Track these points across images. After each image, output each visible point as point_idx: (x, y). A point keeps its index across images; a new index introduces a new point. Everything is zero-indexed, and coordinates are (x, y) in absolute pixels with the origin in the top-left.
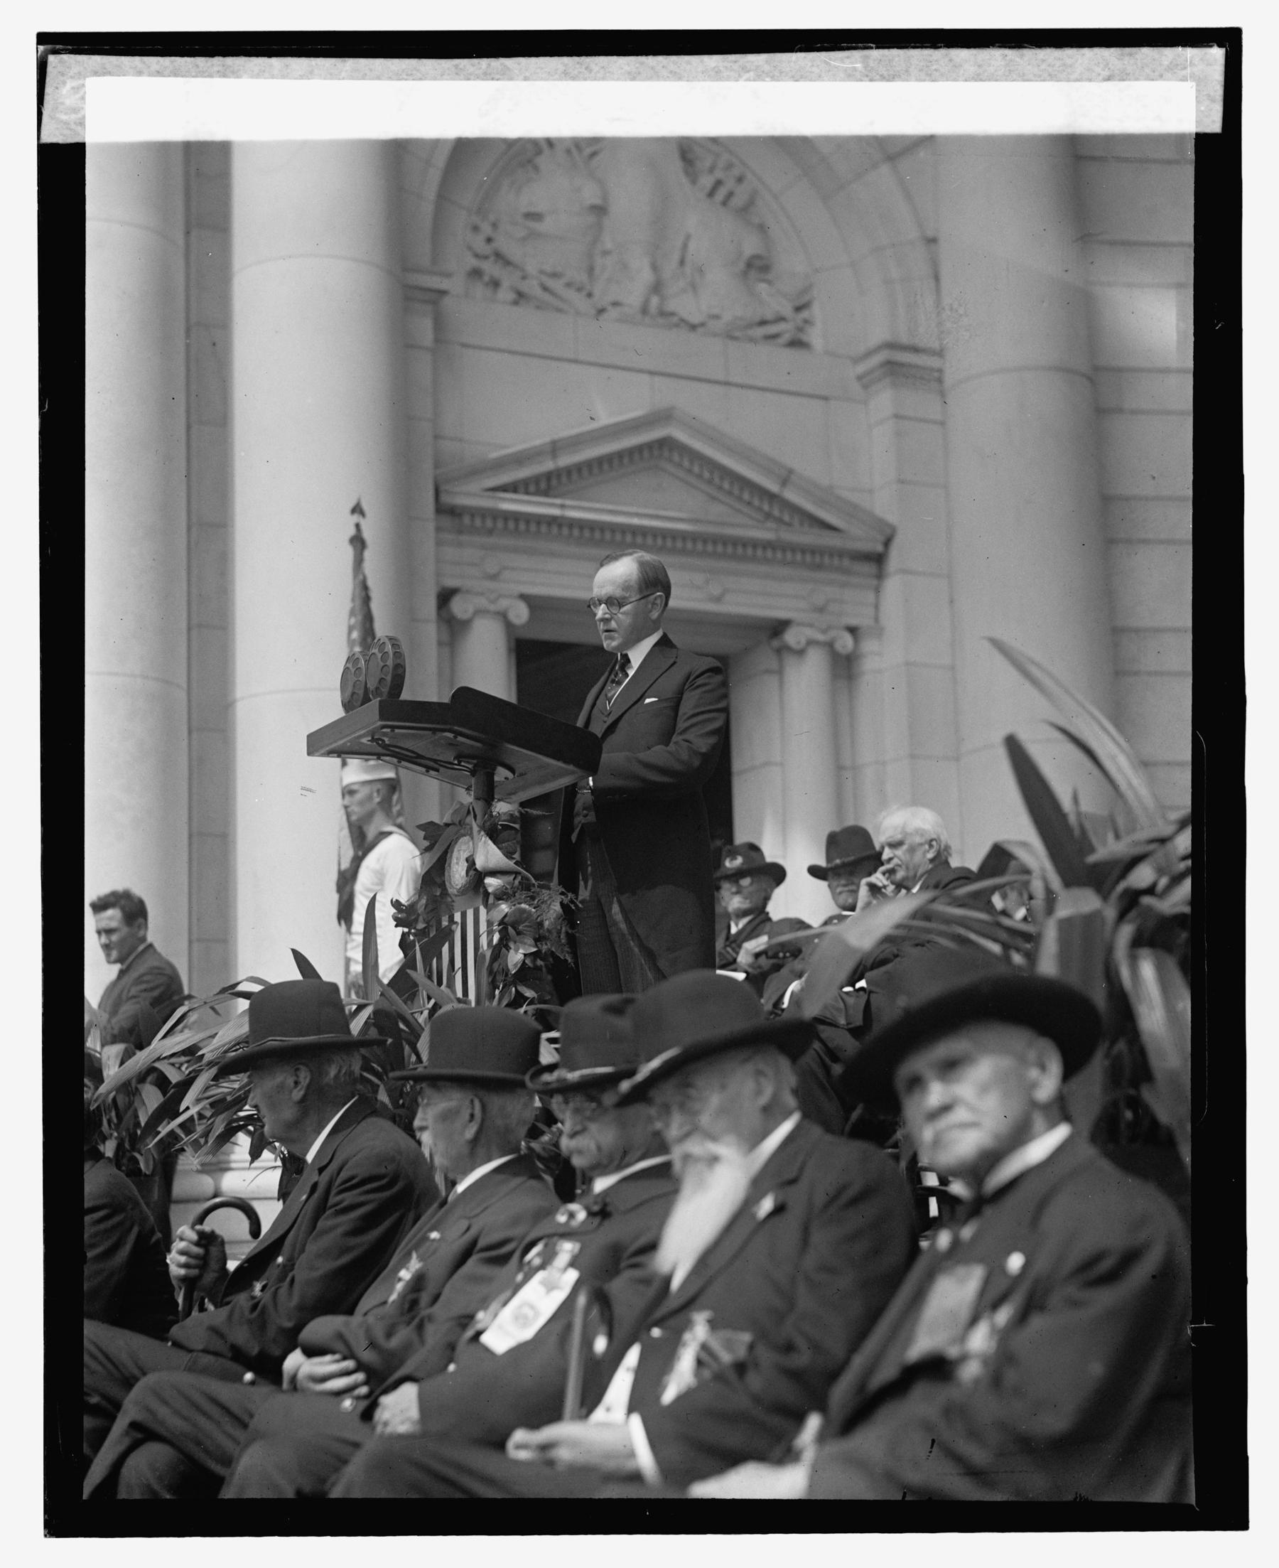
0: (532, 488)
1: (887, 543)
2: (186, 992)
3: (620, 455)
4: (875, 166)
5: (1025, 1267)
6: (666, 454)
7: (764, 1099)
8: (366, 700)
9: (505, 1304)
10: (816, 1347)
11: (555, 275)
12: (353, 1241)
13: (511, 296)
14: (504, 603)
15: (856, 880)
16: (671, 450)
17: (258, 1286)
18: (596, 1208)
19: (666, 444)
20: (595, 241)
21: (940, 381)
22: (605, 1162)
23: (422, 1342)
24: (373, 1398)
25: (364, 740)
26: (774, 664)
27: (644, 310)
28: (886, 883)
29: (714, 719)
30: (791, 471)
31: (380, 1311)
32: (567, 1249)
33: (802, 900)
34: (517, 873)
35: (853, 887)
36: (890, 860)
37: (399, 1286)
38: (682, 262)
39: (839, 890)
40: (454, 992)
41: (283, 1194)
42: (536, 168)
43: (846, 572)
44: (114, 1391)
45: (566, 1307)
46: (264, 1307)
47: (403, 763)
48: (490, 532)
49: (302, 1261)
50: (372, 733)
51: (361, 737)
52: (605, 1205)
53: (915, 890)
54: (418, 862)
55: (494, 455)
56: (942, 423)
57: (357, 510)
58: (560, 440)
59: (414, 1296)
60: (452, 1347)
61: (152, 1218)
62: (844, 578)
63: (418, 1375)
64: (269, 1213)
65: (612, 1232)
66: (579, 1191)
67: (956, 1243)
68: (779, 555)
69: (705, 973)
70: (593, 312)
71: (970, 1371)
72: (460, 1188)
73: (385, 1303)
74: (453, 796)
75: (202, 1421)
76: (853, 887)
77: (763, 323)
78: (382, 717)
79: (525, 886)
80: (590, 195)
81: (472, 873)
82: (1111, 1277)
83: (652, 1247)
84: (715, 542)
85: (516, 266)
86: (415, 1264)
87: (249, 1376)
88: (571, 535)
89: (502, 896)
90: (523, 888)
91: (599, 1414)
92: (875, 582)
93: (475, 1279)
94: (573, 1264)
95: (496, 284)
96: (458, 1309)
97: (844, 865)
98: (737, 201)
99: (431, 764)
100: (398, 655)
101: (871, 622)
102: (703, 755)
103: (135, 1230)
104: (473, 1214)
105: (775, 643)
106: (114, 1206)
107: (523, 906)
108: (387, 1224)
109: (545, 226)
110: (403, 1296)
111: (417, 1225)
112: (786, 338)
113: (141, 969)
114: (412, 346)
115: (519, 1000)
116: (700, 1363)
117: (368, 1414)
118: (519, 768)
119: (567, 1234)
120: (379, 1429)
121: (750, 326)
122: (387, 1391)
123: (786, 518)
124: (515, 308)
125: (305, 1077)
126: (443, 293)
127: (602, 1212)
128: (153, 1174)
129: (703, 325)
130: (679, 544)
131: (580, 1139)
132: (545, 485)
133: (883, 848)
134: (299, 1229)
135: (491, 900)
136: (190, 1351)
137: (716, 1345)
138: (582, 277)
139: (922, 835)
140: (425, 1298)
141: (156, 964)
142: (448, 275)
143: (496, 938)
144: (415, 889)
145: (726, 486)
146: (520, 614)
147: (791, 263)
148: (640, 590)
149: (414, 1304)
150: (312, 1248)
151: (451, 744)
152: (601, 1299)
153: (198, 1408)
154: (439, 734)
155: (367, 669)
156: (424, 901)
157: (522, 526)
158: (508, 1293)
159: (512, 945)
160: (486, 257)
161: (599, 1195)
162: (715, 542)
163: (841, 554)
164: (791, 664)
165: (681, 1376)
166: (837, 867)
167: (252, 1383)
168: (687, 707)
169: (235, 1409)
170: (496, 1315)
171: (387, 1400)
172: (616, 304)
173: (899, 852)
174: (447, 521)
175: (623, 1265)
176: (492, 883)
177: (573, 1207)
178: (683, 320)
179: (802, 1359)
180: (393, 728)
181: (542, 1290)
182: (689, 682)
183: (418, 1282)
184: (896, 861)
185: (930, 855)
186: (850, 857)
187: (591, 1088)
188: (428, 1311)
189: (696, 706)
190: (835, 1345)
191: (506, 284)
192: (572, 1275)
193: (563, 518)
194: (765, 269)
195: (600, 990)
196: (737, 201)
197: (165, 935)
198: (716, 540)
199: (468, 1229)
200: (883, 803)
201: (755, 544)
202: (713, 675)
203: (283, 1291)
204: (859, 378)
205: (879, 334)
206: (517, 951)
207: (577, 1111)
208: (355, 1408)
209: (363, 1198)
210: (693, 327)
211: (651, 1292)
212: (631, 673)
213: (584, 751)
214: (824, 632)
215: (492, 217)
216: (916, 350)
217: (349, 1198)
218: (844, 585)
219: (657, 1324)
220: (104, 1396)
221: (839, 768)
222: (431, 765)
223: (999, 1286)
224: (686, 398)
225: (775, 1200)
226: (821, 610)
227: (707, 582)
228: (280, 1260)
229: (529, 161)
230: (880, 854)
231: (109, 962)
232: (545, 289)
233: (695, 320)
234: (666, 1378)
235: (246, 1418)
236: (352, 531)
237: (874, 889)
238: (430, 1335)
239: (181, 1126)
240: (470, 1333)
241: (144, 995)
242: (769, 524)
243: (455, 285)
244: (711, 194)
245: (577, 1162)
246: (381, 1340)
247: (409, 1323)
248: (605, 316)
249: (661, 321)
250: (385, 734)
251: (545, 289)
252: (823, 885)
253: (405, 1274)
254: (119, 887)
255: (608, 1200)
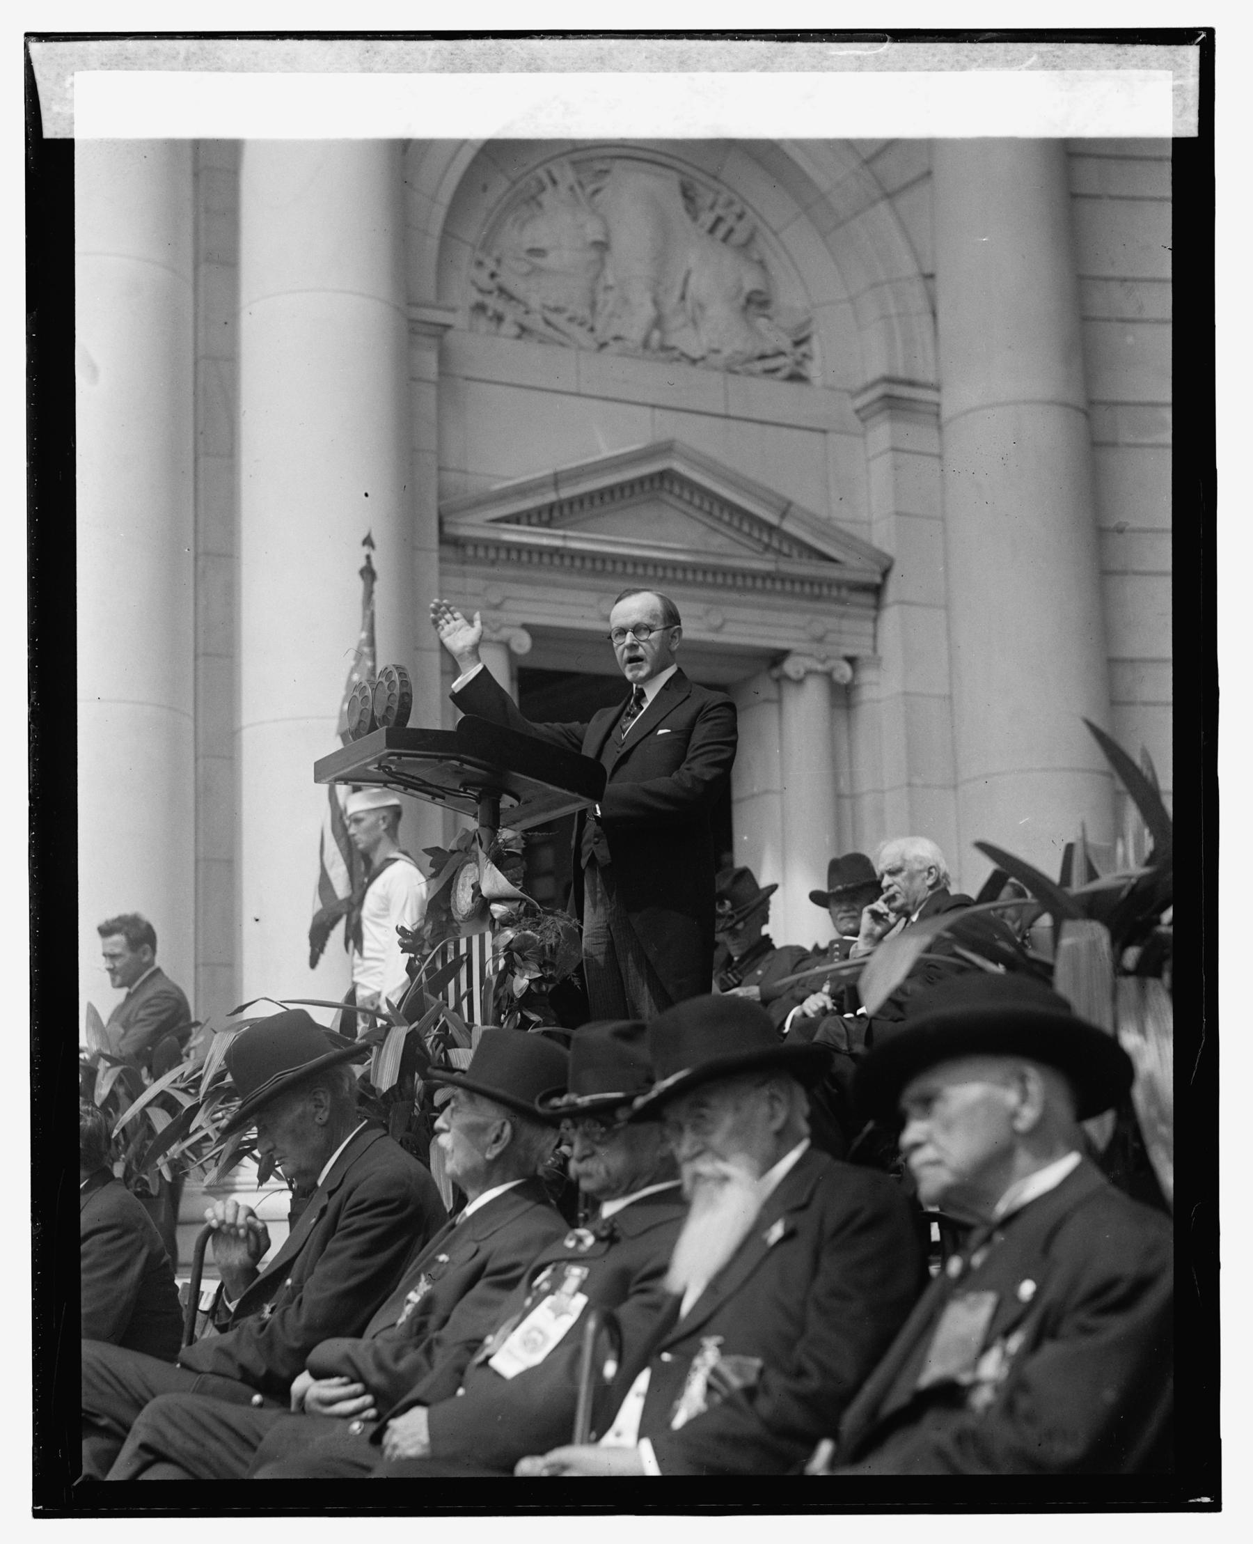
0: (534, 520)
1: (885, 573)
2: (193, 1020)
3: (621, 487)
4: (874, 203)
5: (1037, 1295)
6: (667, 485)
7: (777, 1124)
8: (373, 728)
9: (514, 1328)
10: (825, 1371)
11: (557, 310)
12: (362, 1263)
13: (515, 330)
14: (505, 633)
15: (857, 907)
16: (672, 483)
17: (268, 1308)
18: (604, 1233)
19: (666, 476)
20: (597, 277)
21: (938, 415)
22: (614, 1186)
23: (431, 1366)
24: (382, 1421)
25: (371, 768)
26: (773, 694)
27: (646, 344)
28: (887, 910)
29: (722, 751)
30: (790, 504)
31: (387, 1334)
32: (576, 1274)
33: (796, 922)
34: (522, 900)
35: (855, 914)
36: (890, 886)
37: (408, 1309)
38: (683, 297)
39: (840, 916)
40: (462, 1017)
41: (293, 1218)
42: (540, 205)
43: (843, 602)
44: (123, 1412)
45: (577, 1330)
46: (271, 1330)
47: (410, 790)
48: (493, 563)
49: (310, 1283)
50: (379, 761)
51: (369, 764)
52: (613, 1230)
53: (914, 918)
54: (424, 888)
55: (497, 487)
56: (940, 457)
57: (368, 542)
58: (562, 472)
59: (423, 1318)
60: (461, 1371)
61: (161, 1239)
62: (841, 609)
63: (427, 1399)
64: (279, 1236)
65: (620, 1257)
66: (581, 1215)
67: (967, 1270)
68: (778, 586)
69: (703, 999)
70: (595, 346)
71: (982, 1397)
72: (469, 1210)
73: (394, 1325)
74: (455, 823)
75: (213, 1445)
76: (855, 914)
77: (762, 357)
78: (389, 746)
79: (530, 912)
80: (593, 231)
81: (477, 899)
82: (1124, 1304)
83: (661, 1271)
84: (802, 583)
85: (519, 301)
86: (424, 1287)
87: (257, 1398)
88: (572, 566)
89: (507, 922)
90: (527, 914)
91: (609, 1439)
92: (872, 613)
93: (483, 1303)
94: (581, 1289)
95: (499, 318)
96: (467, 1334)
97: (846, 891)
98: (739, 237)
99: (441, 793)
100: (405, 683)
101: (869, 652)
102: (706, 782)
103: (145, 1252)
104: (481, 1237)
105: (775, 673)
106: (121, 1227)
107: (529, 932)
108: (396, 1247)
109: (550, 261)
110: (411, 1319)
111: (427, 1247)
112: (785, 372)
113: (149, 993)
114: (420, 380)
115: (525, 1024)
116: (710, 1387)
117: (377, 1439)
118: (525, 795)
119: (575, 1259)
120: (388, 1451)
121: (749, 360)
122: (395, 1415)
123: (785, 549)
124: (520, 342)
125: (326, 1099)
126: (447, 327)
127: (610, 1237)
128: (159, 1196)
129: (703, 358)
130: (720, 579)
131: (591, 1165)
132: (548, 516)
133: (882, 876)
134: (307, 1254)
135: (497, 926)
136: (199, 1373)
137: (725, 1370)
138: (584, 312)
139: (921, 862)
140: (433, 1320)
141: (165, 987)
142: (453, 310)
143: (502, 963)
144: (421, 914)
145: (726, 517)
146: (523, 643)
147: (790, 299)
148: (665, 621)
149: (422, 1326)
150: (319, 1270)
151: (456, 772)
152: (611, 1323)
153: (204, 1427)
154: (445, 762)
155: (374, 697)
156: (429, 927)
157: (525, 557)
158: (517, 1318)
159: (517, 971)
160: (490, 292)
161: (607, 1219)
162: (802, 583)
163: (839, 584)
164: (790, 692)
165: (691, 1402)
166: (839, 893)
167: (261, 1405)
168: (697, 739)
169: (244, 1432)
170: (504, 1339)
171: (395, 1424)
172: (617, 338)
173: (898, 879)
174: (450, 552)
175: (632, 1290)
176: (498, 909)
177: (582, 1232)
178: (683, 354)
179: (813, 1383)
180: (399, 755)
181: (551, 1315)
182: (700, 715)
183: (427, 1305)
184: (895, 888)
185: (930, 882)
186: (851, 884)
187: (602, 1113)
188: (436, 1335)
189: (705, 738)
190: (847, 1370)
191: (509, 318)
192: (581, 1300)
193: (564, 548)
194: (765, 304)
195: (609, 1016)
196: (739, 237)
197: (174, 960)
198: (715, 570)
199: (477, 1251)
200: (882, 833)
201: (754, 575)
202: (718, 704)
203: (292, 1311)
204: (857, 411)
205: (877, 368)
206: (522, 977)
207: (586, 1135)
208: (362, 1432)
209: (372, 1222)
210: (694, 361)
211: (660, 1317)
212: (645, 706)
213: (586, 776)
214: (823, 662)
215: (496, 253)
216: (911, 383)
217: (359, 1221)
218: (842, 616)
219: (667, 1349)
220: (114, 1418)
221: (838, 796)
222: (436, 792)
223: (1011, 1313)
224: (697, 436)
225: (786, 1225)
226: (820, 640)
227: (707, 612)
228: (289, 1282)
229: (533, 198)
230: (880, 882)
231: (114, 987)
232: (548, 323)
233: (696, 354)
234: (676, 1403)
235: (253, 1440)
236: (362, 563)
237: (877, 916)
238: (440, 1358)
239: (189, 1148)
240: (480, 1358)
241: (152, 1018)
242: (769, 556)
243: (459, 320)
244: (712, 230)
245: (585, 1185)
246: (389, 1361)
247: (417, 1346)
248: (606, 350)
249: (662, 355)
250: (392, 762)
251: (548, 323)
252: (823, 912)
253: (414, 1297)
254: (127, 910)
255: (616, 1225)
